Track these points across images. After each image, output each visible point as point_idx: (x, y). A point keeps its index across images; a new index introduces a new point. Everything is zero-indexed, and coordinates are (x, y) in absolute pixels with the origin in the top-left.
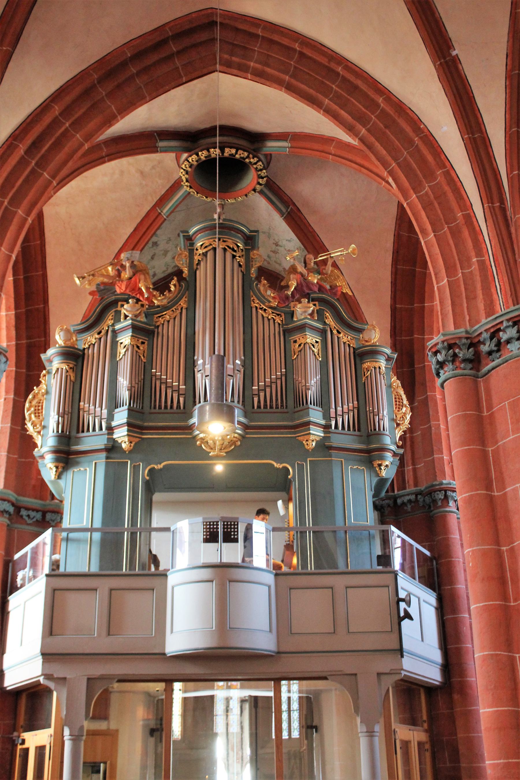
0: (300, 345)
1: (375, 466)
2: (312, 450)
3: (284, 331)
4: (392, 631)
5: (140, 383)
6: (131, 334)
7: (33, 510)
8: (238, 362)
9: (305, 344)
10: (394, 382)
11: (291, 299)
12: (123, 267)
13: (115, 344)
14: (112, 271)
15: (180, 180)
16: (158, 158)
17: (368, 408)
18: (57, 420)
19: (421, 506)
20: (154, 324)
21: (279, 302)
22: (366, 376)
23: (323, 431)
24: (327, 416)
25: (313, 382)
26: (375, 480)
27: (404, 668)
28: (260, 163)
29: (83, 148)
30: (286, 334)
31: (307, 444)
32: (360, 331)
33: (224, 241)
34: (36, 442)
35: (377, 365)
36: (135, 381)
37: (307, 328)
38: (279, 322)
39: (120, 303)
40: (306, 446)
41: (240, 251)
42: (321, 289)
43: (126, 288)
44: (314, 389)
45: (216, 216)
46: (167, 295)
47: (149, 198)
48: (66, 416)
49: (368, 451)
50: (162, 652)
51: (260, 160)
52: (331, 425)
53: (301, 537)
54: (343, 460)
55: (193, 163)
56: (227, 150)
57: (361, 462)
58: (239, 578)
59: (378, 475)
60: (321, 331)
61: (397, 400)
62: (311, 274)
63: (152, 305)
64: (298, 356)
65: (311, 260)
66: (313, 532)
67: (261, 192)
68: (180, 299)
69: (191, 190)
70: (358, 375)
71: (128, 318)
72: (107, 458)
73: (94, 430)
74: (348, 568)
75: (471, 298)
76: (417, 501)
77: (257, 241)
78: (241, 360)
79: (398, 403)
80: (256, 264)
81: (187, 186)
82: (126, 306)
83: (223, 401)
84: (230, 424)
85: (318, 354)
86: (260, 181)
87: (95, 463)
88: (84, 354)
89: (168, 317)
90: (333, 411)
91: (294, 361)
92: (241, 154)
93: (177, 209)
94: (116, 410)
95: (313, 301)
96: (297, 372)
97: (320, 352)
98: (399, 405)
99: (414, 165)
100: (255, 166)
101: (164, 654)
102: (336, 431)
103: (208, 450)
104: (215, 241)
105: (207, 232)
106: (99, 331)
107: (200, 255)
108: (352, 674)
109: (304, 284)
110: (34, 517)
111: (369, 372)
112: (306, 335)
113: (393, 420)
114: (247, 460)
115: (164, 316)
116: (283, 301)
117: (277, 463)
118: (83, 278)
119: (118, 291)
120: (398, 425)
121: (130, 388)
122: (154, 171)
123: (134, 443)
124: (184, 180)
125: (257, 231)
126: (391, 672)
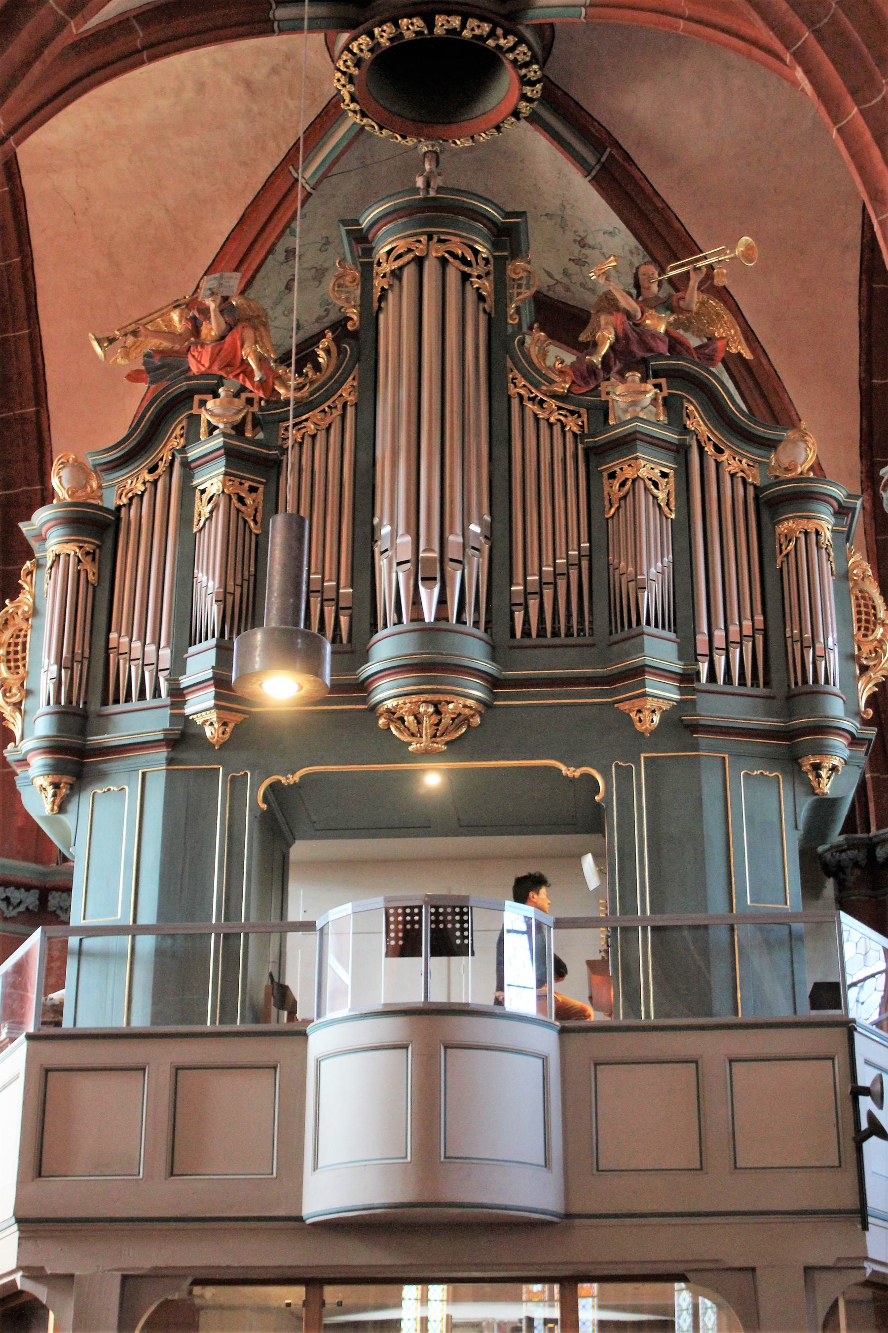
0: (623, 484)
1: (804, 769)
2: (652, 733)
3: (587, 451)
4: (840, 1166)
5: (246, 584)
6: (223, 469)
7: (18, 886)
8: (475, 528)
9: (634, 481)
10: (856, 565)
11: (601, 374)
12: (205, 312)
13: (188, 492)
14: (180, 321)
15: (337, 99)
16: (283, 48)
17: (788, 629)
18: (55, 675)
20: (280, 442)
21: (573, 382)
22: (784, 553)
23: (680, 688)
24: (687, 652)
25: (653, 570)
26: (805, 805)
27: (872, 1254)
28: (523, 48)
29: (65, 32)
30: (592, 457)
31: (640, 720)
32: (771, 445)
33: (440, 241)
34: (12, 727)
35: (811, 526)
36: (235, 579)
37: (638, 442)
38: (576, 429)
39: (197, 398)
40: (639, 724)
41: (482, 263)
42: (675, 345)
43: (212, 362)
44: (656, 587)
45: (420, 182)
46: (310, 374)
47: (271, 145)
48: (77, 667)
49: (788, 735)
50: (294, 1214)
51: (522, 40)
52: (698, 673)
53: (624, 940)
54: (726, 756)
55: (362, 55)
56: (440, 20)
57: (772, 760)
58: (484, 1040)
59: (812, 791)
60: (674, 448)
61: (863, 609)
62: (650, 312)
63: (273, 400)
64: (618, 508)
65: (650, 278)
66: (654, 929)
67: (534, 118)
68: (341, 383)
69: (365, 120)
70: (767, 551)
71: (216, 432)
72: (170, 761)
73: (142, 696)
74: (736, 1014)
77: (523, 237)
78: (481, 523)
79: (863, 617)
80: (519, 294)
81: (355, 112)
82: (210, 404)
83: (297, 624)
84: (311, 678)
85: (668, 505)
86: (528, 90)
87: (144, 774)
88: (118, 519)
89: (312, 426)
90: (702, 639)
91: (610, 521)
92: (475, 28)
93: (335, 170)
94: (192, 650)
95: (656, 376)
96: (616, 548)
97: (672, 499)
98: (867, 621)
99: (856, 35)
100: (511, 56)
101: (300, 1219)
102: (712, 687)
103: (405, 738)
104: (420, 241)
105: (400, 221)
106: (151, 465)
107: (384, 276)
108: (745, 1269)
109: (633, 336)
110: (20, 903)
111: (792, 544)
112: (636, 458)
113: (853, 658)
114: (496, 760)
115: (305, 424)
116: (583, 378)
117: (568, 766)
118: (112, 341)
119: (194, 368)
120: (864, 669)
121: (221, 598)
122: (276, 79)
123: (231, 725)
124: (347, 98)
125: (521, 214)
126: (839, 1265)
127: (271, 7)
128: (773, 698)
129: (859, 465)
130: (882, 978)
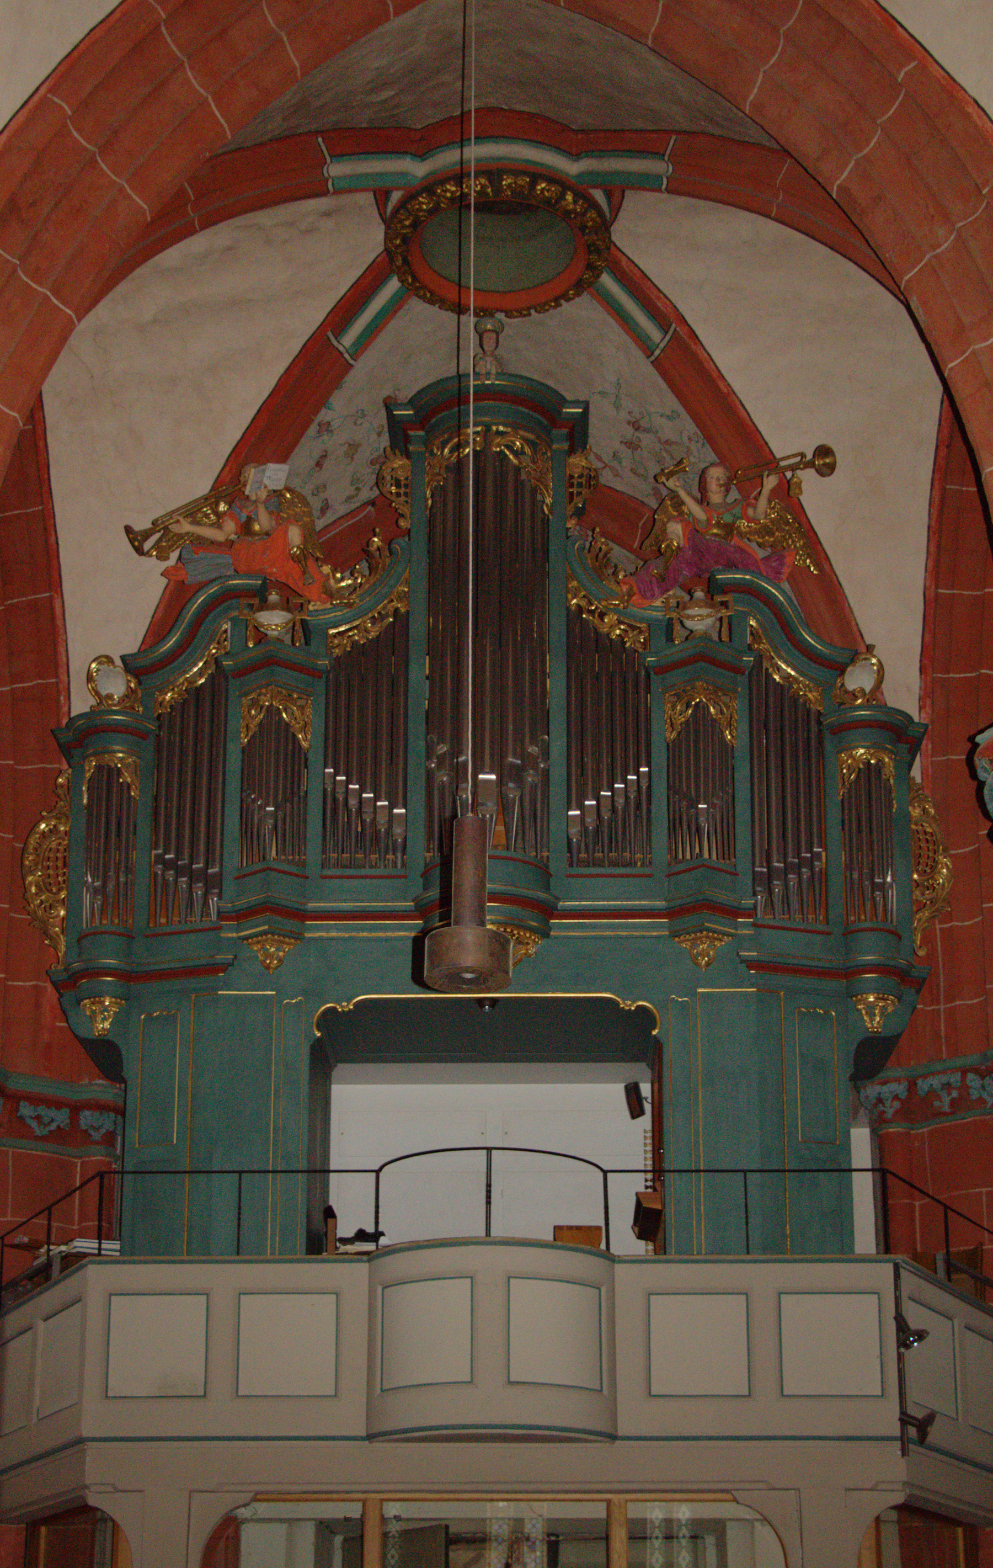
19: (974, 1098)
75: (860, 849)
76: (964, 1088)
127: (326, 163)
128: (829, 934)
129: (918, 680)
130: (8, 1333)
